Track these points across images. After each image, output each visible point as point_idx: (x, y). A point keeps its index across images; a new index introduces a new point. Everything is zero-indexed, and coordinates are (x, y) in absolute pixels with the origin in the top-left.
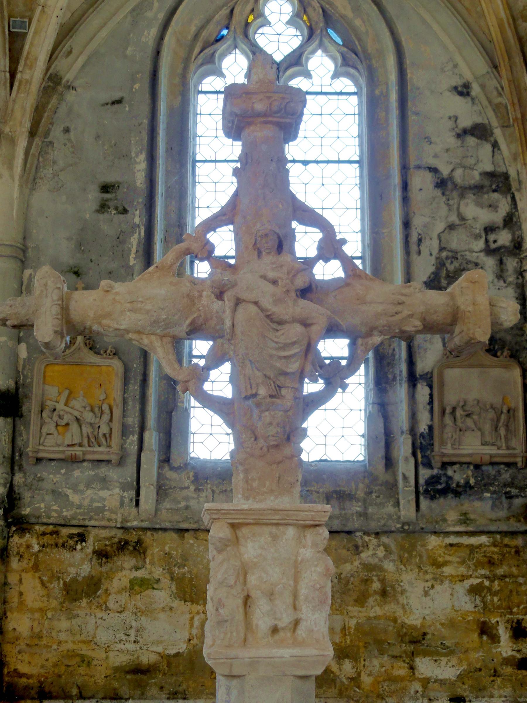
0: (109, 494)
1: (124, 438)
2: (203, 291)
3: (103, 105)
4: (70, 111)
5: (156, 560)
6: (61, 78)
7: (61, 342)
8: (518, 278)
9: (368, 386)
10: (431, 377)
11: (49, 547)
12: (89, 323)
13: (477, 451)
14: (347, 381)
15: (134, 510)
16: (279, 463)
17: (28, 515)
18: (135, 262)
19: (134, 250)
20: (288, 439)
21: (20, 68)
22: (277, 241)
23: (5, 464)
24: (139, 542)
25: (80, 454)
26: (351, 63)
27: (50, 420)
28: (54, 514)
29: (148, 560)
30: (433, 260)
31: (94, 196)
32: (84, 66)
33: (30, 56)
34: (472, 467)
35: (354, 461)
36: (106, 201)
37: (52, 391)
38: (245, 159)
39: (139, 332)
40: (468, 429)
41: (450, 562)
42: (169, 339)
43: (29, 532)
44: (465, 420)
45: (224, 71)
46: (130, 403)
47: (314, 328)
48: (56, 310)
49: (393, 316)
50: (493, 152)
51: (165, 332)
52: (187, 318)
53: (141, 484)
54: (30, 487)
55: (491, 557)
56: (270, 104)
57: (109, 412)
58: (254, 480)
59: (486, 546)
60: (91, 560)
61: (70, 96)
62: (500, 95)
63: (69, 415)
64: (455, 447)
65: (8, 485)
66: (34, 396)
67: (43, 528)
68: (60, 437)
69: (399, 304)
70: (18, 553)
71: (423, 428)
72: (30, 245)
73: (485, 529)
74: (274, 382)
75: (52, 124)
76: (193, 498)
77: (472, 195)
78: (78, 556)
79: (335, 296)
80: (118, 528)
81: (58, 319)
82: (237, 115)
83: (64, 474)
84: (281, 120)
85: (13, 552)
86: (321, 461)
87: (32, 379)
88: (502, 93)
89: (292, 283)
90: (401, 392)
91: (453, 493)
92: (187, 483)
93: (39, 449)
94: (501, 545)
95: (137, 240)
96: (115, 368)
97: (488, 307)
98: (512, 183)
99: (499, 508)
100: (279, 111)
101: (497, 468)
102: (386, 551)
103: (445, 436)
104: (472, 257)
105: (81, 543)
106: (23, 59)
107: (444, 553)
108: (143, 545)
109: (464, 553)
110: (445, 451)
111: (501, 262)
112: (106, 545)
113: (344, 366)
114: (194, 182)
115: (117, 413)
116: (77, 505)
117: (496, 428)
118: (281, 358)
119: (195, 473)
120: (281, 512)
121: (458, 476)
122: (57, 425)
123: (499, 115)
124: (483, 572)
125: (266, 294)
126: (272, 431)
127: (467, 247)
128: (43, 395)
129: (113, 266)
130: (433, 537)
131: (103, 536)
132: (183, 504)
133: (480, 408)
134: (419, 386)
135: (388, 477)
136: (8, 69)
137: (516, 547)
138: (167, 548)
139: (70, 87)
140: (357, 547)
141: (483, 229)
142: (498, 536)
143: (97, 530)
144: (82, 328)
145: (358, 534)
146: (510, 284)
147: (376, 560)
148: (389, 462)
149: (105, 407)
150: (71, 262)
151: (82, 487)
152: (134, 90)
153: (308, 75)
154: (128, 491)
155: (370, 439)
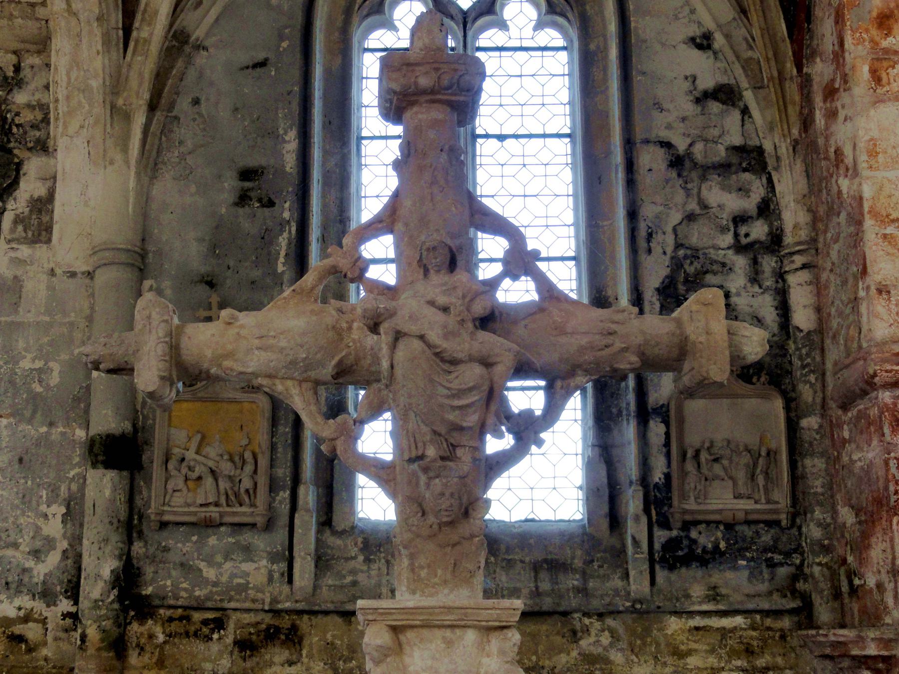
0: (253, 567)
1: (273, 495)
2: (353, 321)
3: (242, 69)
4: (201, 75)
5: (315, 651)
6: (189, 36)
7: (171, 391)
8: (777, 282)
9: (586, 424)
10: (668, 411)
11: (178, 636)
12: (206, 366)
13: (729, 507)
14: (543, 435)
15: (286, 588)
16: (454, 545)
17: (150, 595)
18: (285, 269)
19: (283, 253)
20: (466, 514)
21: (136, 24)
22: (449, 256)
23: (120, 530)
24: (294, 628)
25: (215, 516)
26: (558, 10)
27: (176, 472)
28: (184, 594)
29: (304, 652)
30: (667, 260)
31: (230, 184)
32: (217, 20)
33: (148, 9)
34: (722, 528)
35: (569, 521)
36: (247, 190)
37: (179, 436)
38: (408, 148)
39: (270, 376)
40: (716, 477)
41: (696, 650)
42: (310, 385)
43: (152, 618)
44: (712, 466)
45: (396, 23)
46: (280, 450)
47: (499, 369)
48: (161, 349)
49: (602, 349)
50: (743, 120)
51: (305, 375)
52: (333, 357)
53: (296, 553)
54: (153, 559)
55: (748, 644)
56: (439, 78)
57: (253, 462)
58: (422, 567)
59: (742, 629)
60: (232, 653)
61: (201, 59)
62: (751, 48)
63: (202, 467)
64: (700, 501)
65: (124, 558)
66: (156, 442)
67: (169, 613)
68: (190, 494)
69: (610, 334)
70: (138, 645)
71: (657, 476)
72: (151, 248)
73: (740, 607)
74: (446, 440)
75: (177, 94)
76: (362, 572)
77: (716, 177)
78: (215, 647)
79: (526, 326)
80: (266, 611)
81: (165, 361)
82: (395, 93)
83: (196, 542)
84: (453, 98)
85: (131, 643)
86: (527, 520)
87: (154, 420)
88: (753, 44)
89: (468, 310)
90: (629, 431)
91: (697, 561)
92: (354, 551)
93: (163, 511)
94: (761, 628)
95: (286, 241)
96: (261, 405)
97: (726, 338)
98: (768, 160)
99: (757, 580)
100: (448, 88)
101: (753, 527)
102: (612, 637)
103: (687, 487)
104: (718, 256)
105: (219, 632)
106: (140, 13)
107: (688, 639)
108: (299, 633)
109: (714, 639)
110: (687, 507)
111: (755, 262)
112: (250, 634)
113: (538, 417)
114: (360, 165)
115: (263, 462)
116: (213, 581)
117: (753, 477)
118: (454, 408)
119: (365, 539)
120: (456, 611)
121: (704, 539)
122: (186, 479)
123: (749, 73)
124: (739, 663)
125: (434, 326)
126: (445, 503)
127: (710, 243)
128: (168, 440)
129: (256, 274)
130: (673, 618)
131: (246, 622)
132: (349, 579)
133: (732, 451)
134: (652, 424)
135: (614, 541)
136: (120, 25)
137: (782, 630)
138: (329, 637)
139: (200, 47)
140: (574, 633)
141: (730, 219)
142: (758, 617)
143: (238, 614)
144: (197, 372)
145: (576, 615)
146: (767, 289)
147: (600, 650)
148: (615, 521)
149: (248, 455)
150: (203, 270)
151: (219, 558)
152: (281, 49)
153: (503, 26)
154: (278, 563)
155: (591, 493)
